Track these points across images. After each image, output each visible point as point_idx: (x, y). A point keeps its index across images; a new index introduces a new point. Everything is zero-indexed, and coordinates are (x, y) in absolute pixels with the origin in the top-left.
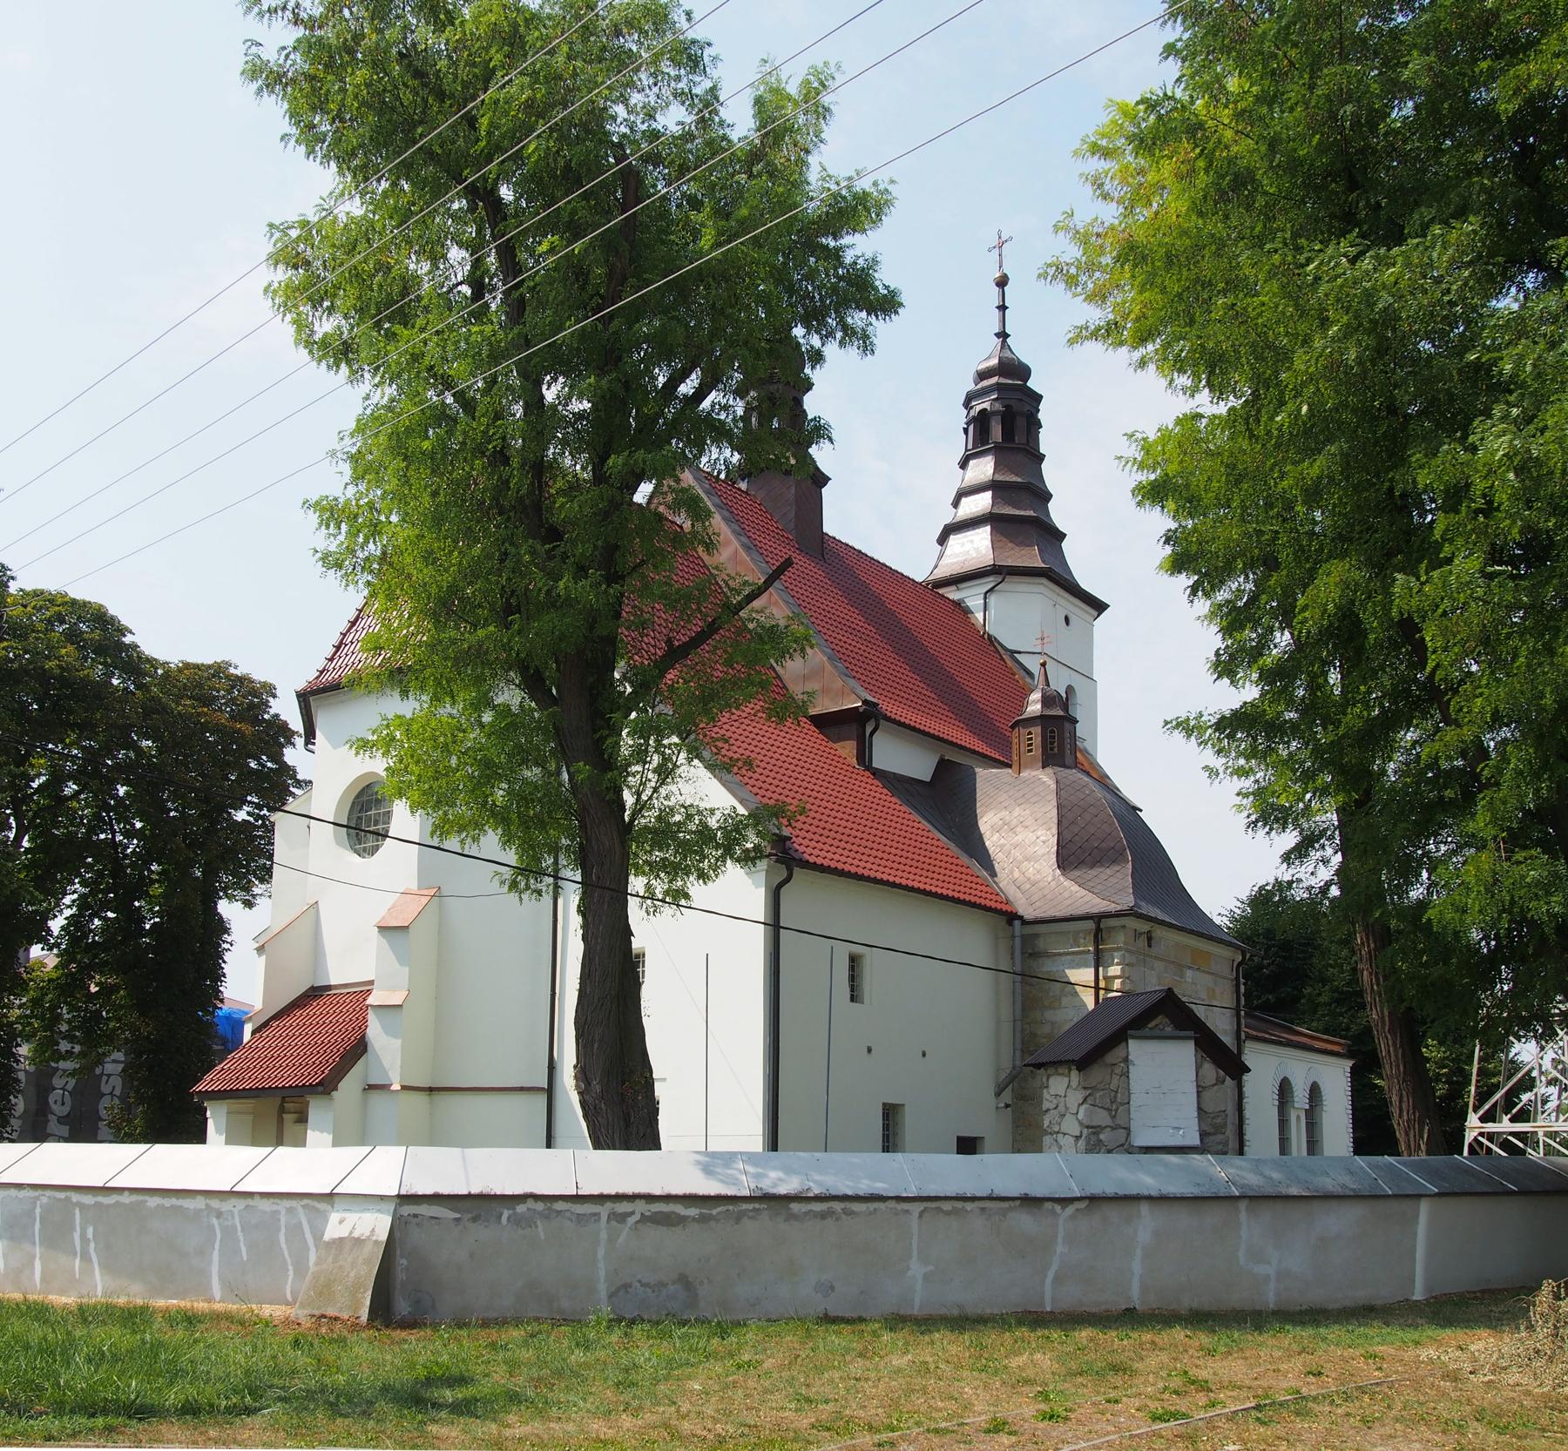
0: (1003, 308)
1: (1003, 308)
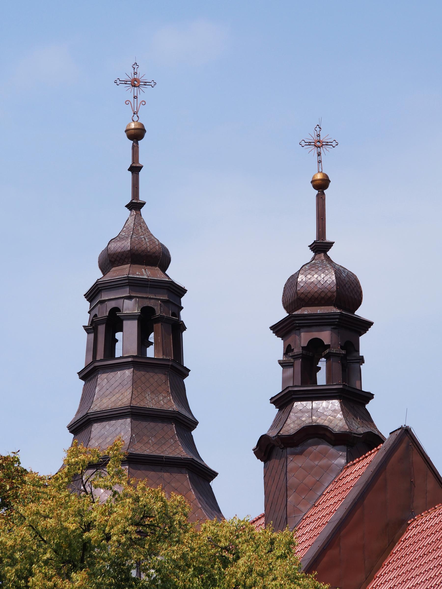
0: (320, 162)
1: (320, 162)
